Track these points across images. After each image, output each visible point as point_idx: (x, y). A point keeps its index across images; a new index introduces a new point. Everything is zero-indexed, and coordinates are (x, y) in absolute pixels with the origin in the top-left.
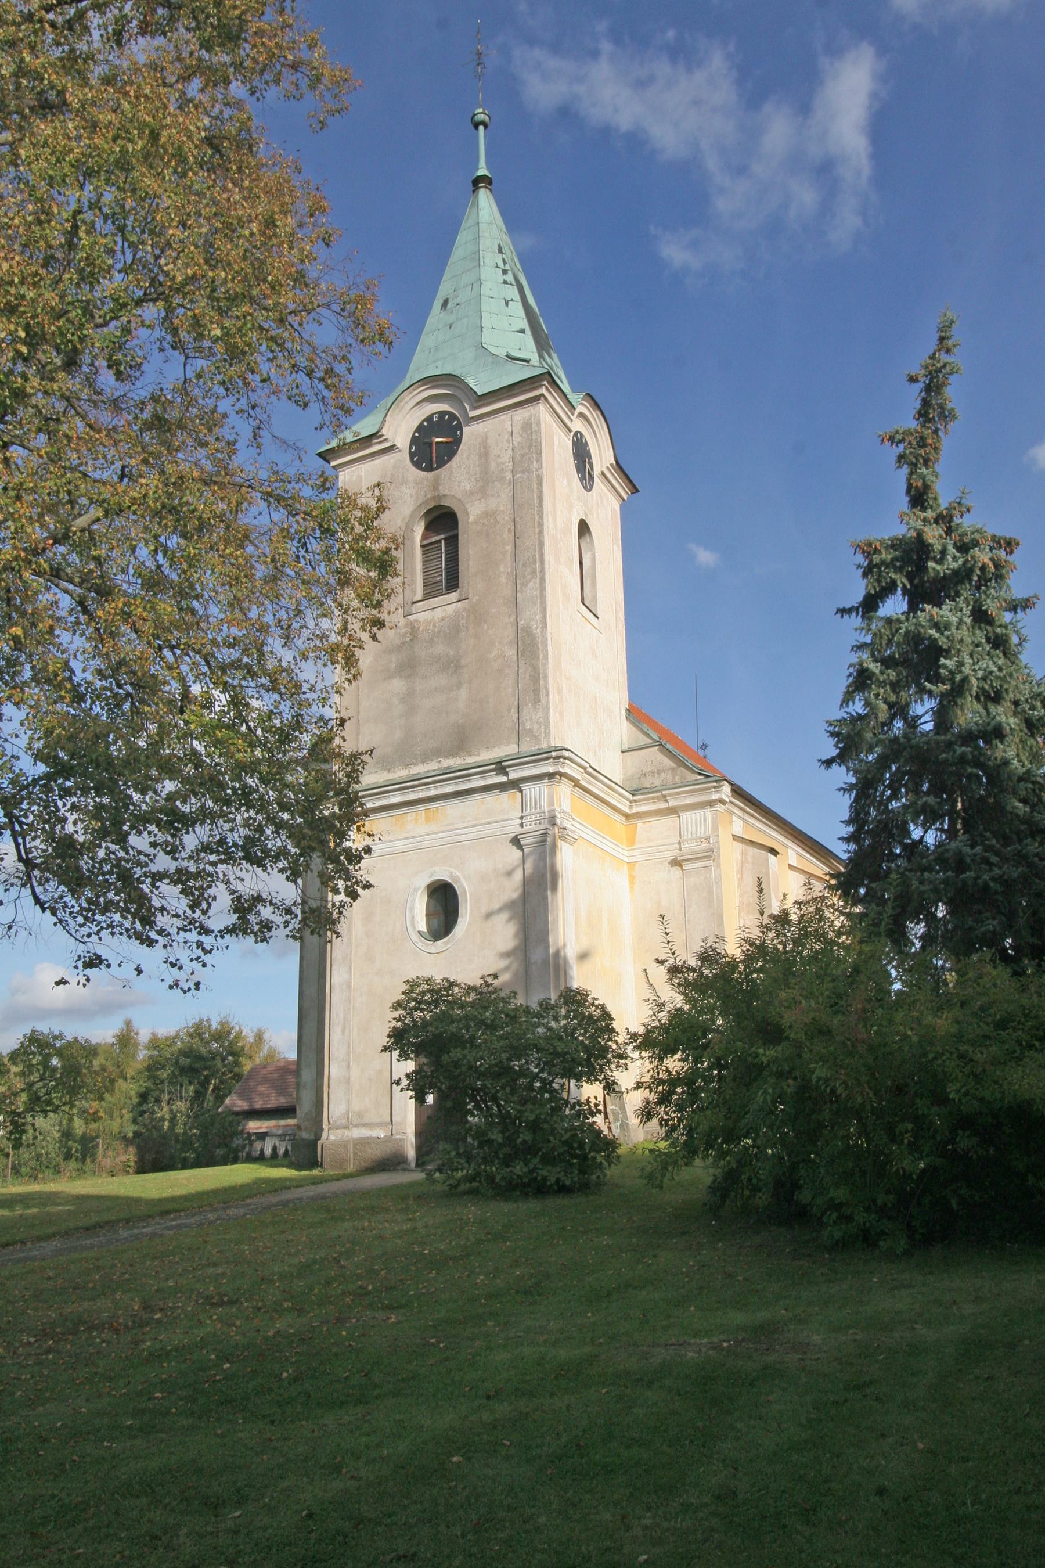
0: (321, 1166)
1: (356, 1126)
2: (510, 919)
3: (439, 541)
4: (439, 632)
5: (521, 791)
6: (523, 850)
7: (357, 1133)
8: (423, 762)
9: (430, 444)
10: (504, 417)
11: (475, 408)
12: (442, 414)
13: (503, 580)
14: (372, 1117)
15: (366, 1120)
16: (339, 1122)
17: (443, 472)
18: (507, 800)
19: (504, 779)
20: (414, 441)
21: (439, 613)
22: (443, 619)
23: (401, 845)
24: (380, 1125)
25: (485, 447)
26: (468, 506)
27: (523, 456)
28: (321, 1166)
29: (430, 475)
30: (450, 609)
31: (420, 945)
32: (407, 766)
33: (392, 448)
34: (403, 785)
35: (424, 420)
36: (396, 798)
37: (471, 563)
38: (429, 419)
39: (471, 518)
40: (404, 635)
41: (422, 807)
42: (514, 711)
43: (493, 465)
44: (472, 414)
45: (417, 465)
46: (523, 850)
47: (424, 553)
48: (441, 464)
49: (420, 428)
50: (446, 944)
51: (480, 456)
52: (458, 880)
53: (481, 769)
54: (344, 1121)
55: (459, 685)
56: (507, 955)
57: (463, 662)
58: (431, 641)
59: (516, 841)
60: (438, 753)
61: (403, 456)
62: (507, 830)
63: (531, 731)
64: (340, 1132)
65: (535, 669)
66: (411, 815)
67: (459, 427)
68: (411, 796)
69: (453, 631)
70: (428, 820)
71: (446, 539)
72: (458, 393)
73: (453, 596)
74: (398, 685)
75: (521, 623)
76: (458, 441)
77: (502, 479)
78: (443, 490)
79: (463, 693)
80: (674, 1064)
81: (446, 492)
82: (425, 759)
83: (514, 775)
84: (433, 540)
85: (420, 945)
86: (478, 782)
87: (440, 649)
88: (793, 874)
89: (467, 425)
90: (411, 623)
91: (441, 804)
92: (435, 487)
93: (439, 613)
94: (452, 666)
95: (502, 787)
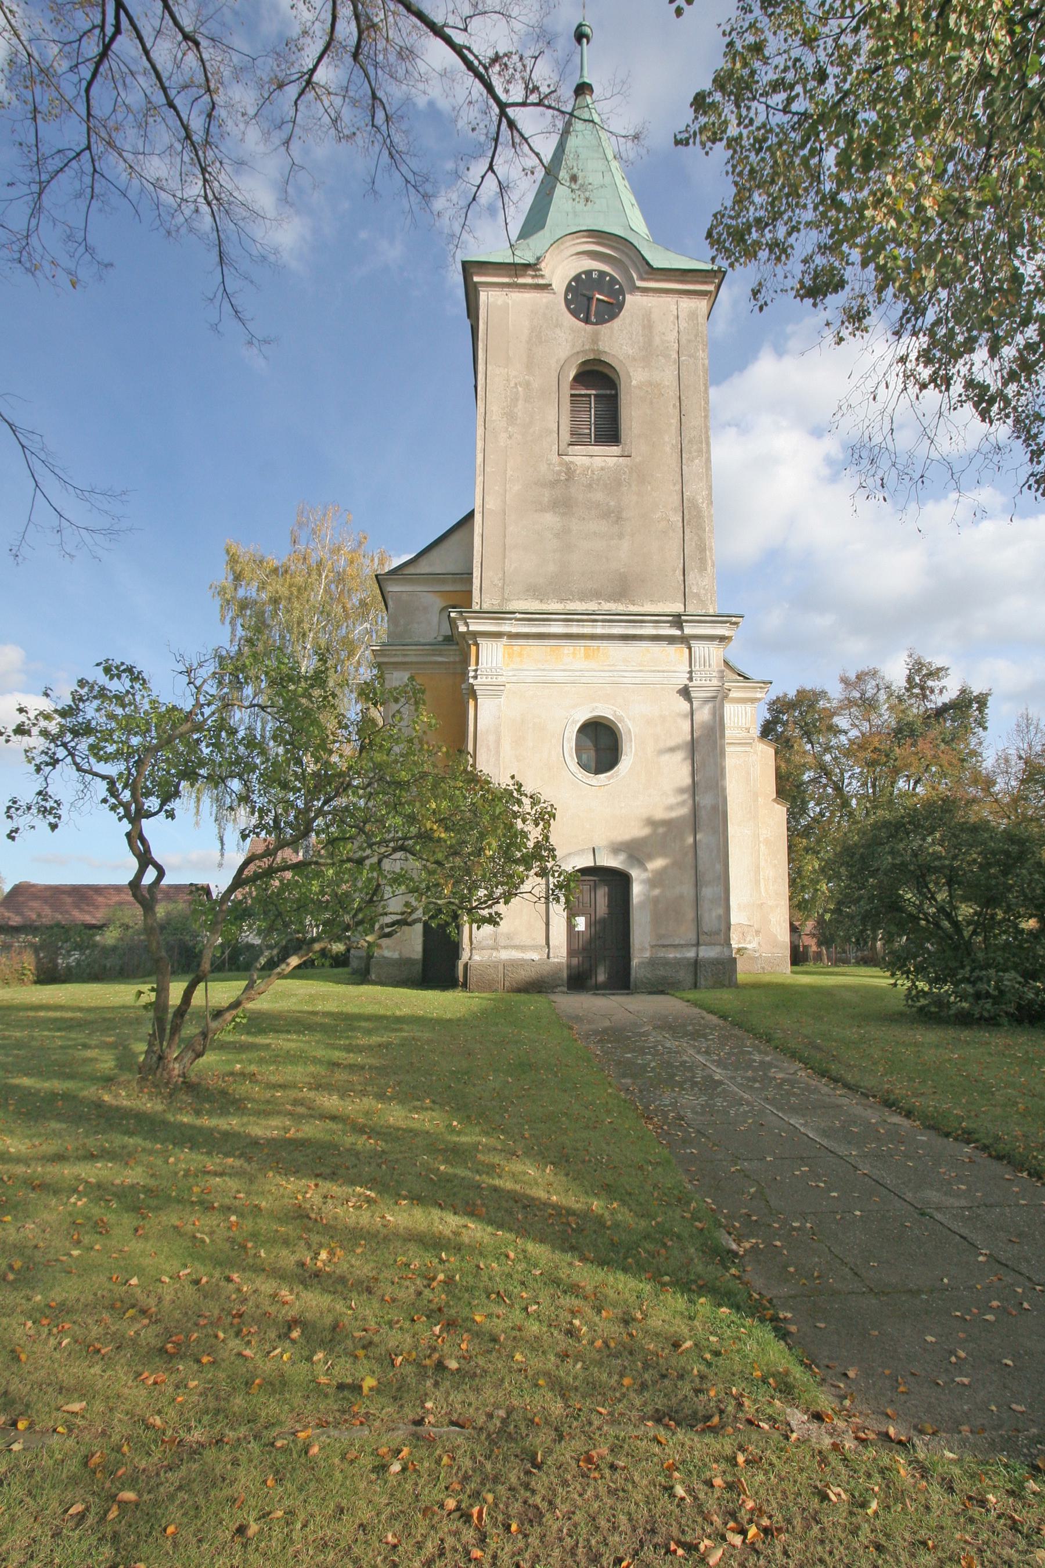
0: (465, 985)
1: (505, 947)
2: (685, 759)
3: (589, 396)
4: (598, 480)
5: (690, 648)
6: (691, 703)
7: (505, 955)
8: (581, 600)
9: (590, 299)
10: (670, 300)
11: (642, 279)
12: (602, 274)
13: (668, 449)
14: (524, 939)
15: (517, 942)
16: (484, 943)
17: (604, 329)
18: (676, 654)
19: (678, 633)
20: (569, 288)
21: (598, 462)
22: (602, 469)
23: (558, 676)
24: (534, 948)
25: (649, 321)
26: (631, 370)
27: (689, 341)
28: (465, 985)
29: (589, 328)
30: (611, 462)
31: (579, 776)
32: (562, 600)
33: (546, 287)
34: (569, 617)
35: (584, 272)
36: (599, 630)
37: (634, 425)
38: (588, 273)
39: (634, 383)
40: (559, 473)
41: (582, 642)
42: (679, 573)
43: (657, 341)
44: (639, 284)
45: (575, 313)
46: (691, 703)
47: (572, 402)
48: (601, 321)
49: (577, 278)
50: (609, 778)
51: (644, 327)
52: (622, 720)
53: (656, 618)
54: (491, 942)
55: (621, 536)
56: (681, 791)
57: (624, 515)
58: (590, 486)
59: (685, 693)
60: (596, 595)
61: (557, 299)
62: (674, 681)
63: (697, 595)
64: (486, 953)
65: (701, 539)
66: (568, 648)
67: (621, 292)
68: (574, 629)
69: (614, 483)
70: (587, 657)
71: (596, 396)
72: (624, 259)
73: (615, 450)
74: (550, 519)
75: (686, 494)
76: (621, 306)
77: (667, 357)
78: (602, 346)
79: (625, 544)
80: (657, 892)
81: (607, 349)
82: (583, 597)
83: (688, 630)
84: (583, 392)
85: (579, 776)
86: (649, 630)
87: (599, 496)
88: (666, 758)
89: (631, 293)
90: (567, 464)
91: (605, 644)
92: (595, 339)
93: (598, 462)
94: (614, 516)
95: (671, 640)
